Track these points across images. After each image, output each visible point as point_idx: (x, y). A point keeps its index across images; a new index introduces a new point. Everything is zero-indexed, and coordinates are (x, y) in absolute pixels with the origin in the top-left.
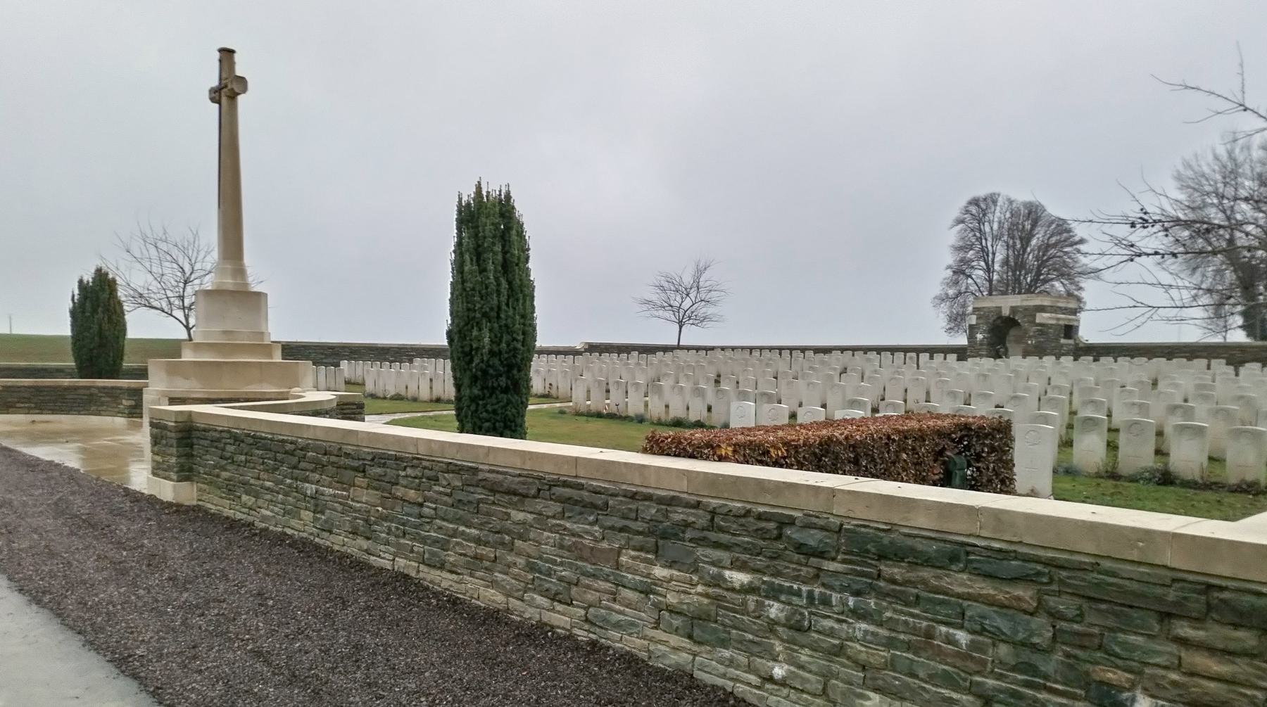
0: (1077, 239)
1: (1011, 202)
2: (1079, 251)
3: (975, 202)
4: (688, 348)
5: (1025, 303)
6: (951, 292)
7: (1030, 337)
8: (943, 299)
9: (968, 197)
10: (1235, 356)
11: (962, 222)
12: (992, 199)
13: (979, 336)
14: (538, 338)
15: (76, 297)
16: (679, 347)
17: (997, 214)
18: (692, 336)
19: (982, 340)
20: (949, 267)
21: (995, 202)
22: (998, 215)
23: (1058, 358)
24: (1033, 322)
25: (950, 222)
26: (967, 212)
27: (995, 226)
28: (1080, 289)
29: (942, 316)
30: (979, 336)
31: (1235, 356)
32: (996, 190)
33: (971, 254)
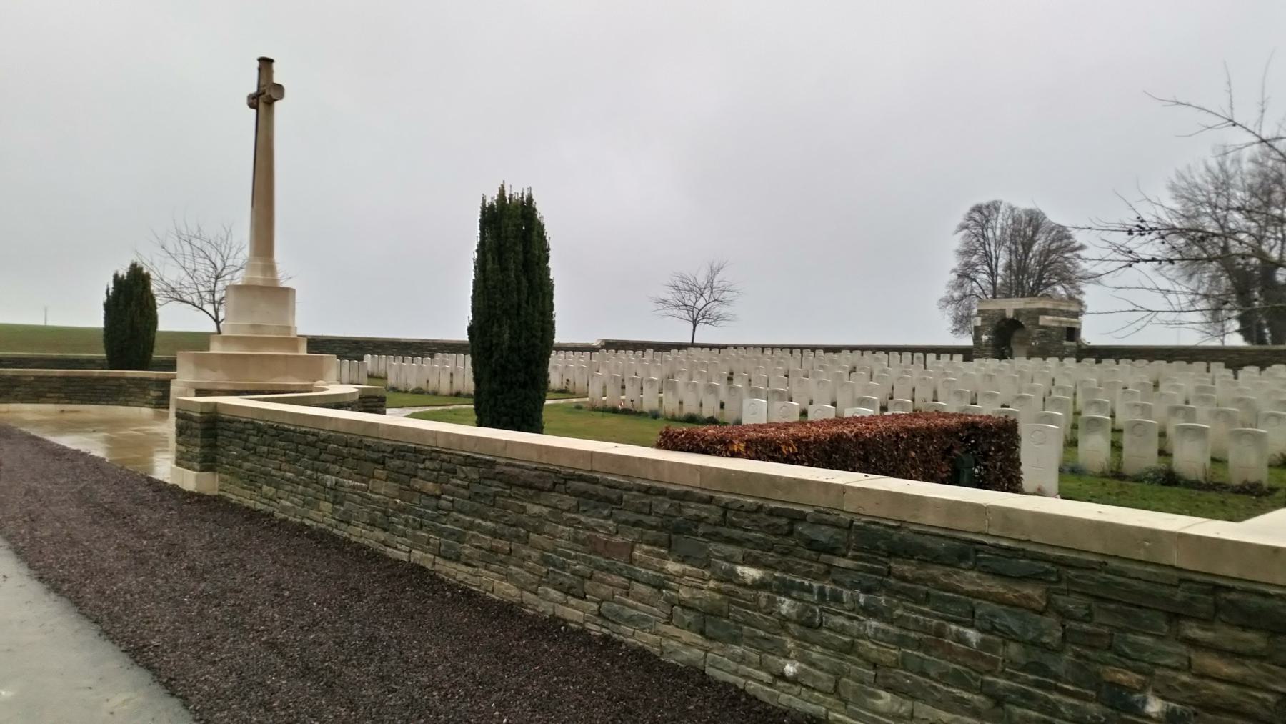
0: (1077, 245)
1: (1013, 210)
2: (1079, 257)
3: (978, 209)
4: (702, 346)
6: (956, 295)
7: (1034, 339)
8: (949, 301)
12: (994, 207)
13: (985, 338)
16: (693, 345)
17: (1000, 220)
18: (706, 334)
20: (954, 271)
21: (997, 209)
22: (1000, 222)
23: (1061, 360)
24: (1036, 325)
25: (955, 228)
26: (971, 218)
27: (998, 232)
28: (1081, 293)
29: (948, 317)
30: (985, 338)
31: (968, 354)
33: (975, 259)
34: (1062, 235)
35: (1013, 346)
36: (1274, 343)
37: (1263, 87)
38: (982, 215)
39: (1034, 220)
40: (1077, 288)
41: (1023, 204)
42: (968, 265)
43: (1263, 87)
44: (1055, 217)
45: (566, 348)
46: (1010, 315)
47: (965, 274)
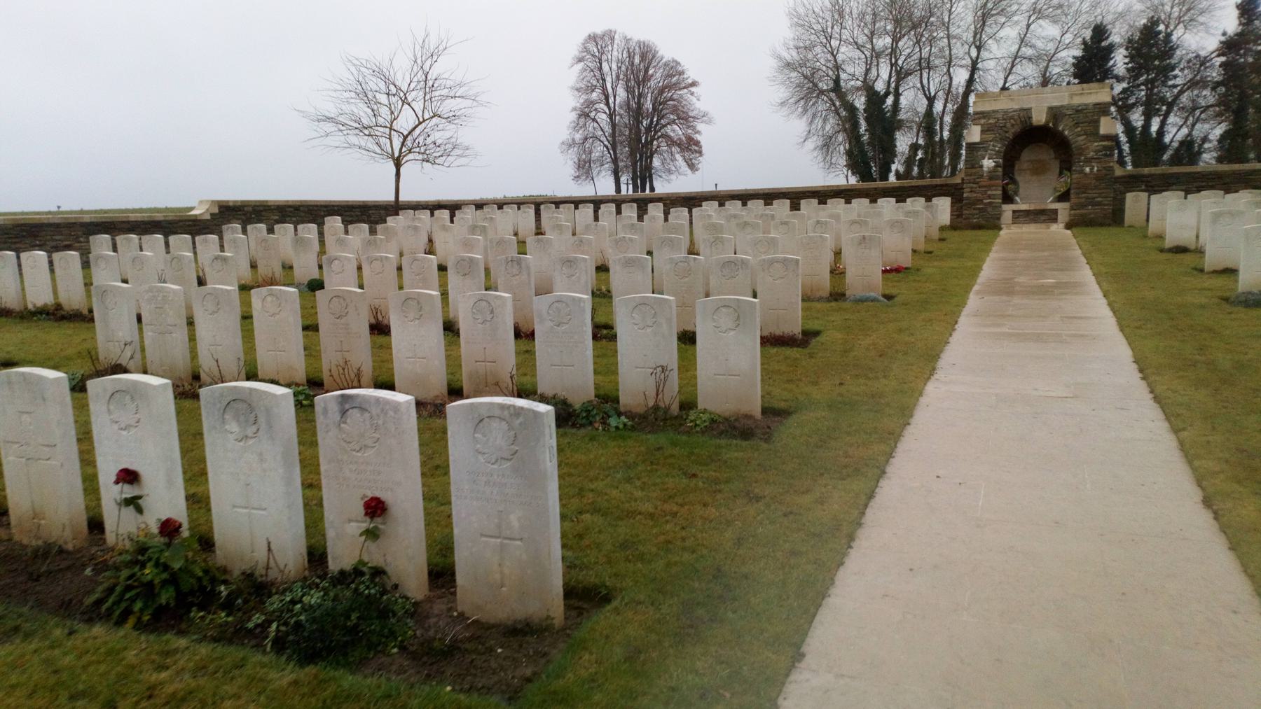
0: (690, 81)
1: (628, 40)
2: (692, 94)
3: (593, 38)
4: (417, 206)
5: (1077, 101)
6: (578, 137)
7: (1089, 161)
8: (571, 144)
9: (585, 35)
10: (846, 194)
11: (580, 60)
12: (610, 36)
13: (988, 163)
14: (1129, 374)
15: (193, 213)
16: (395, 208)
17: (615, 53)
18: (421, 183)
19: (992, 171)
20: (574, 109)
21: (612, 39)
22: (616, 52)
23: (929, 199)
24: (1094, 134)
25: (570, 61)
26: (586, 50)
27: (614, 66)
28: (698, 132)
29: (570, 163)
30: (988, 163)
31: (846, 194)
32: (613, 28)
33: (594, 96)
34: (673, 70)
35: (1018, 178)
36: (1135, 165)
37: (21, 274)
38: (598, 44)
39: (647, 54)
40: (694, 128)
41: (639, 33)
42: (590, 103)
43: (21, 274)
44: (666, 51)
45: (18, 258)
46: (1039, 118)
47: (585, 114)
